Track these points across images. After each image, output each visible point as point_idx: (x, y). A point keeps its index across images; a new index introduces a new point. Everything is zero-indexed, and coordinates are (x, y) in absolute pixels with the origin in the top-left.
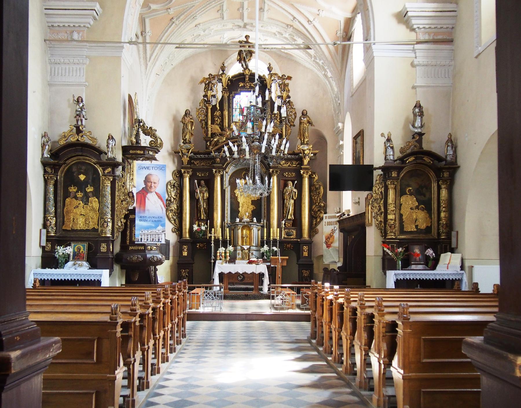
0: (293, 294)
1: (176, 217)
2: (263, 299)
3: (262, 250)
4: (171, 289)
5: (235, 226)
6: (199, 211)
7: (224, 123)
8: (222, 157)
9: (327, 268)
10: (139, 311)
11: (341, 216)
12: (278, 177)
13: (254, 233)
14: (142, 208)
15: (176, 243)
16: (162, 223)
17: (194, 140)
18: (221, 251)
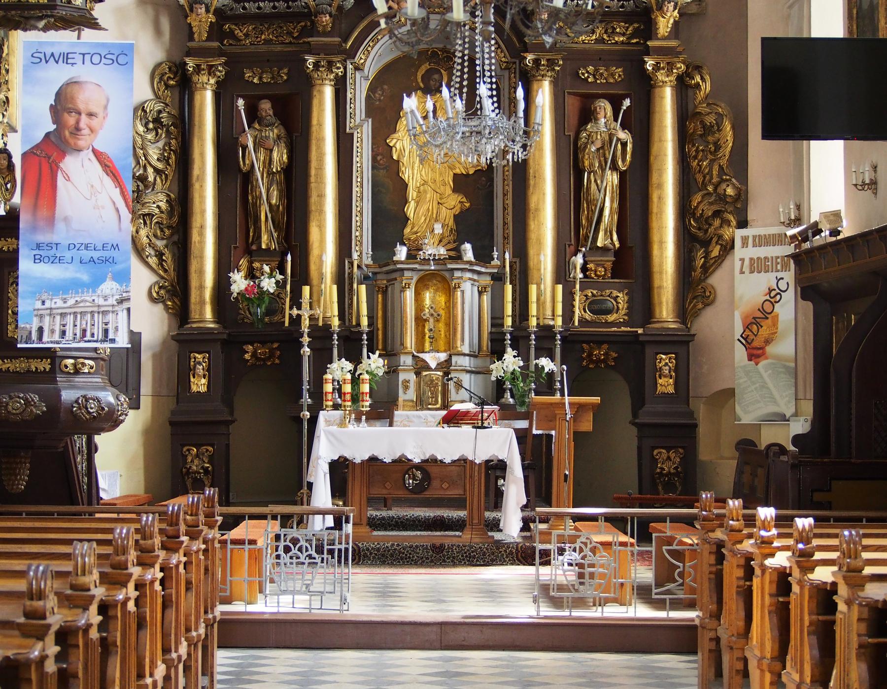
1: (164, 242)
3: (498, 369)
5: (393, 276)
6: (251, 216)
10: (56, 619)
11: (804, 237)
12: (555, 83)
14: (43, 212)
15: (164, 343)
16: (118, 267)
18: (338, 375)
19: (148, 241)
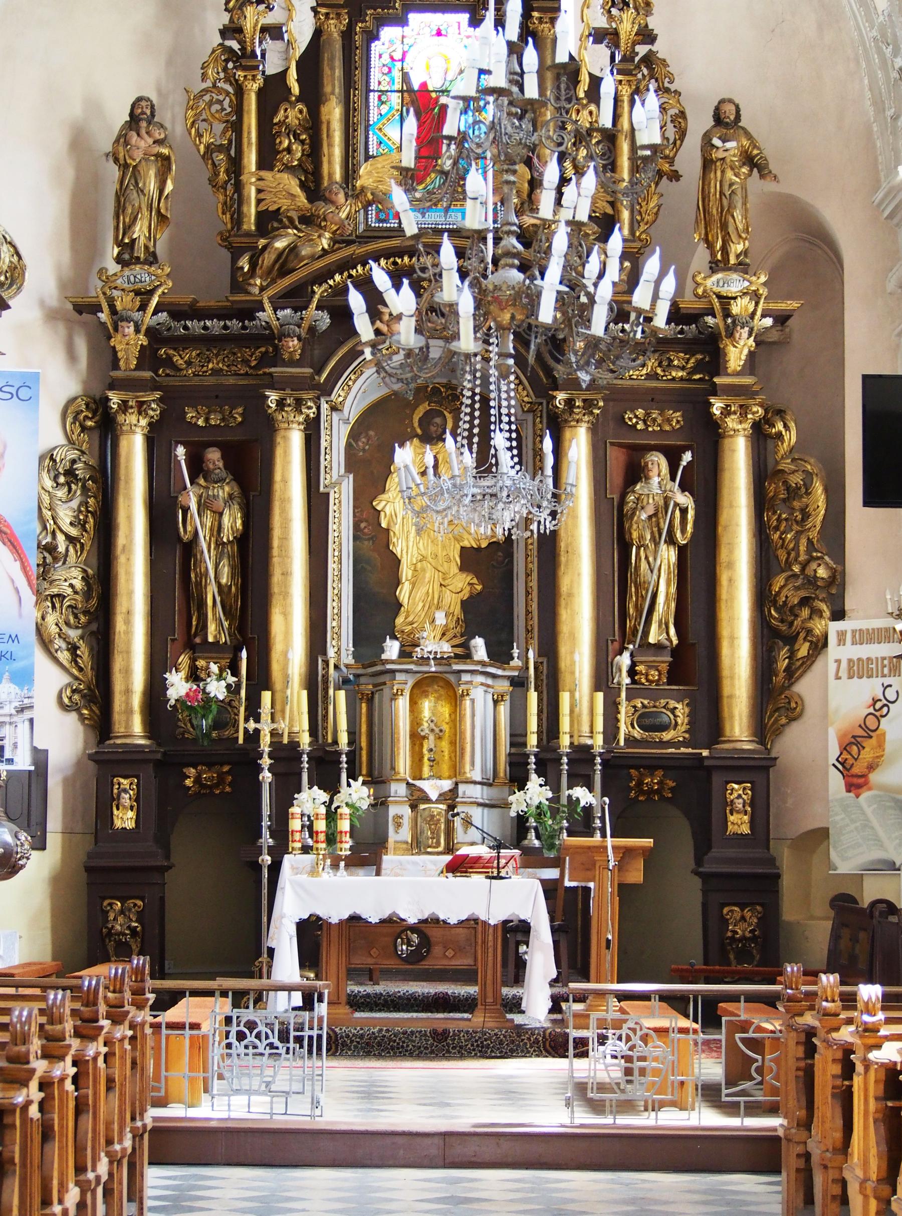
0: (683, 1031)
1: (79, 632)
2: (525, 1054)
3: (518, 802)
4: (77, 1005)
5: (381, 679)
7: (325, 160)
8: (312, 329)
9: (852, 899)
12: (594, 430)
13: (473, 715)
15: (79, 764)
17: (174, 246)
18: (309, 809)
19: (58, 630)
